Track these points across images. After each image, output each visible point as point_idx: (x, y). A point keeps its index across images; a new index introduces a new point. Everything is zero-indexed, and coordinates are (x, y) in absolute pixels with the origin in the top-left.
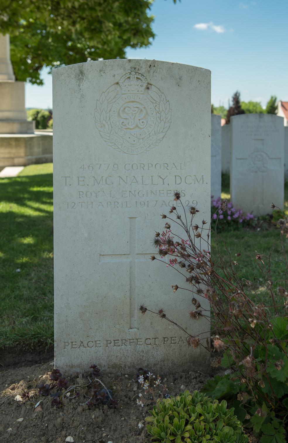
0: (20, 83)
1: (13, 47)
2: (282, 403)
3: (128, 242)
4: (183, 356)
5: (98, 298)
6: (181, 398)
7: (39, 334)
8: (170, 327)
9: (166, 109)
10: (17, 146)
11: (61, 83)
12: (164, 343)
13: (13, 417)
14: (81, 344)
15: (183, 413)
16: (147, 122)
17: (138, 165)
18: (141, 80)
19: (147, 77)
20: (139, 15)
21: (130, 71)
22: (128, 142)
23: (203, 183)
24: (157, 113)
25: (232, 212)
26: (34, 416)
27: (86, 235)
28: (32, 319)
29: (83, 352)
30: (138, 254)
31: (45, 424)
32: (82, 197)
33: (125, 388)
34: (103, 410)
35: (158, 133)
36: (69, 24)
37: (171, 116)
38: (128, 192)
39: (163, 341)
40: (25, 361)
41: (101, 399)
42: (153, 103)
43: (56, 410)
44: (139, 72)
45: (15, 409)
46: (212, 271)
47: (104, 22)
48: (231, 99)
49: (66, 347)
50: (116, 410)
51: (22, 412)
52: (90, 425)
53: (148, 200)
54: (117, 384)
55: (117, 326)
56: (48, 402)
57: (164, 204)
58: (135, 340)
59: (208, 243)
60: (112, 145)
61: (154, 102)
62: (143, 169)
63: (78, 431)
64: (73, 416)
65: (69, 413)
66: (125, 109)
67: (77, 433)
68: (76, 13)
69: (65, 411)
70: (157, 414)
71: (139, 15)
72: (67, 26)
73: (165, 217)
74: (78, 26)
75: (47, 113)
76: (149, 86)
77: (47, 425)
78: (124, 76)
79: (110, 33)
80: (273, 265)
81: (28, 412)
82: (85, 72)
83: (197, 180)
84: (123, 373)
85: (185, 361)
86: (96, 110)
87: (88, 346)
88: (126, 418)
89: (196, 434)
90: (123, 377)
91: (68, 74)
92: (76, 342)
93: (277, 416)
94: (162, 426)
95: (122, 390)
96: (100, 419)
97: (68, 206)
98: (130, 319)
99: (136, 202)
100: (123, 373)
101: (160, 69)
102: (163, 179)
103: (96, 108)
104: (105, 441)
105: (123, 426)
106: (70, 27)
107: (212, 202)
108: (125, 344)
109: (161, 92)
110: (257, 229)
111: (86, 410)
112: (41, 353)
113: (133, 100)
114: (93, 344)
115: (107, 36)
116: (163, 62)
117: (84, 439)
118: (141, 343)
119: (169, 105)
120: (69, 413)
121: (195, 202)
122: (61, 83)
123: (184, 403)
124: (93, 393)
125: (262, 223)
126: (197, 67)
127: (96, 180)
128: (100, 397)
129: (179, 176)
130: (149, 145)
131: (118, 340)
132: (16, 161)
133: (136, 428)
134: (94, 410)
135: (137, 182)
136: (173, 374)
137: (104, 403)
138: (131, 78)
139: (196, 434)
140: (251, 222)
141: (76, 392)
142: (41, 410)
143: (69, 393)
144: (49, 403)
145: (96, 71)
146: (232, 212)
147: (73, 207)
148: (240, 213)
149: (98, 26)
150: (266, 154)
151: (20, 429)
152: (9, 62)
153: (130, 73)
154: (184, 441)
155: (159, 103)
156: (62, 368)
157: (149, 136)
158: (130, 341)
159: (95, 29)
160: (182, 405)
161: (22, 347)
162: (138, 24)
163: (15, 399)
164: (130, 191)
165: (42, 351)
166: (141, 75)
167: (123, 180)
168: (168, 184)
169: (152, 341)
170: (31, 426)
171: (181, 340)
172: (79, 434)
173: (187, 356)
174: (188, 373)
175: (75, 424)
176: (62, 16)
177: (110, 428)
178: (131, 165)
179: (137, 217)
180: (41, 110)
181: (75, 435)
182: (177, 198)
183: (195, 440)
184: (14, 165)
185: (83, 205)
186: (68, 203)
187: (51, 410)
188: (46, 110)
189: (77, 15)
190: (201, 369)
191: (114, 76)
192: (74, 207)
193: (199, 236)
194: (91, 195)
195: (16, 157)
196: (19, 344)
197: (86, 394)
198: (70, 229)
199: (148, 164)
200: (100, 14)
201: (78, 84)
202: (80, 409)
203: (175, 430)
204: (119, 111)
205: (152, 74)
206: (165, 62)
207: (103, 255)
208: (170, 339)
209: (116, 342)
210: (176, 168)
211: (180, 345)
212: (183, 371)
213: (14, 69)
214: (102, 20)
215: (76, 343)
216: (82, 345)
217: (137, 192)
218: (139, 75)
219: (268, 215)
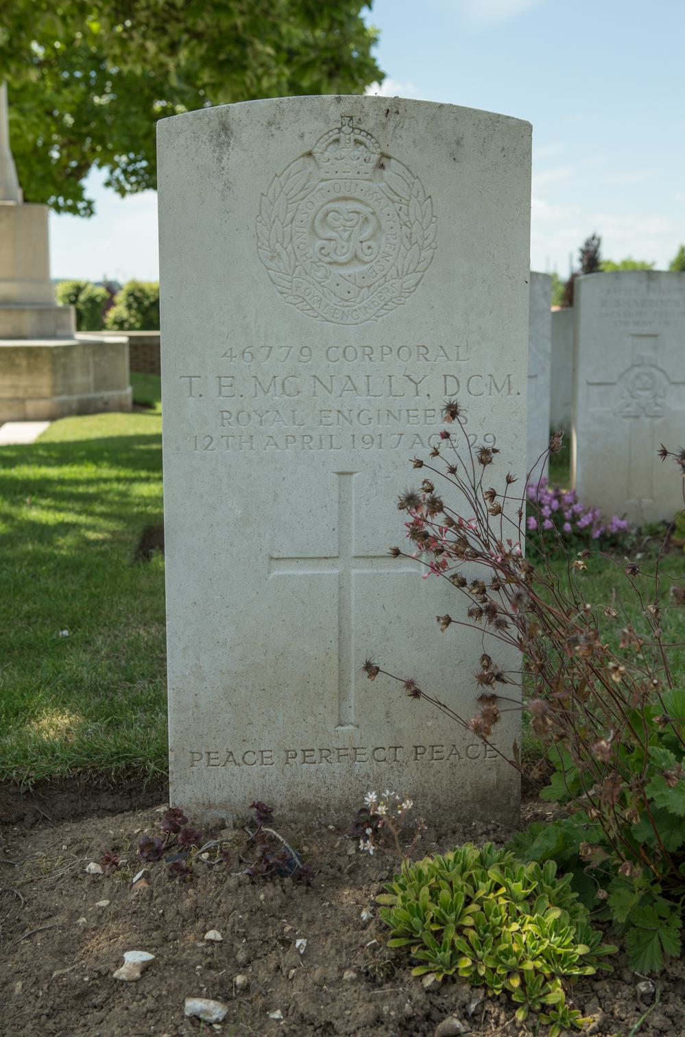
0: (35, 208)
1: (15, 116)
2: (678, 869)
3: (334, 529)
4: (459, 788)
5: (265, 655)
6: (456, 855)
7: (126, 750)
8: (429, 724)
9: (423, 218)
10: (31, 370)
11: (178, 154)
12: (416, 759)
13: (86, 900)
14: (229, 757)
15: (459, 882)
16: (379, 247)
17: (357, 349)
18: (366, 147)
19: (381, 140)
20: (342, 24)
21: (339, 125)
22: (335, 295)
23: (509, 393)
24: (404, 227)
25: (574, 514)
26: (132, 897)
27: (239, 512)
28: (108, 725)
29: (233, 775)
30: (356, 557)
31: (158, 910)
32: (229, 423)
33: (328, 850)
34: (282, 886)
35: (404, 273)
36: (161, 50)
37: (436, 232)
38: (334, 414)
39: (414, 753)
40: (99, 808)
41: (278, 865)
42: (393, 202)
43: (181, 885)
44: (361, 127)
45: (89, 886)
46: (529, 567)
47: (251, 44)
48: (578, 255)
49: (195, 763)
50: (309, 888)
51: (106, 890)
52: (255, 912)
53: (380, 432)
54: (311, 842)
55: (310, 719)
56: (160, 872)
57: (418, 440)
58: (349, 751)
59: (519, 528)
60: (298, 301)
61: (397, 198)
62: (370, 358)
63: (231, 920)
64: (217, 896)
65: (208, 889)
66: (327, 215)
67: (229, 925)
68: (178, 20)
69: (199, 887)
70: (403, 887)
71: (342, 24)
72: (157, 54)
73: (419, 464)
74: (183, 54)
75: (101, 291)
76: (384, 161)
77: (161, 911)
78: (326, 137)
79: (268, 73)
80: (671, 628)
81: (118, 891)
82: (233, 127)
83: (496, 386)
84: (323, 823)
85: (463, 798)
86: (259, 218)
87: (245, 763)
88: (333, 903)
89: (488, 921)
90: (324, 830)
91: (194, 133)
92: (217, 752)
93: (665, 895)
94: (415, 905)
95: (322, 853)
96: (278, 902)
97: (196, 444)
98: (339, 705)
99: (353, 436)
100: (323, 823)
101: (410, 118)
102: (416, 384)
103: (260, 212)
104: (290, 939)
105: (328, 916)
106: (163, 58)
107: (528, 487)
108: (328, 758)
109: (413, 175)
110: (635, 555)
111: (245, 884)
112: (134, 793)
113: (348, 194)
114: (255, 757)
115: (259, 79)
116: (417, 103)
117: (245, 936)
118: (364, 758)
119: (432, 206)
120: (208, 889)
121: (490, 438)
122: (178, 154)
123: (462, 862)
124: (258, 854)
125: (648, 541)
126: (499, 116)
127: (260, 383)
128: (276, 860)
129: (453, 376)
130: (383, 303)
131: (313, 750)
132: (31, 407)
133: (356, 919)
134: (264, 885)
135: (356, 389)
136: (435, 826)
137: (283, 874)
138: (342, 141)
139: (488, 921)
140: (620, 538)
141: (221, 852)
142: (146, 886)
143: (207, 854)
144: (162, 873)
145: (259, 125)
146: (574, 514)
147: (207, 447)
148: (594, 517)
149: (236, 52)
150: (661, 370)
151: (103, 920)
152: (7, 154)
153: (339, 129)
154: (462, 934)
155: (407, 202)
156: (187, 809)
157: (382, 281)
158: (338, 753)
159: (228, 62)
160: (459, 866)
161: (91, 778)
162: (339, 46)
163: (87, 870)
164: (339, 411)
165: (135, 788)
166: (365, 134)
167: (321, 383)
168: (428, 395)
169: (388, 754)
170: (129, 914)
171: (454, 752)
172: (234, 926)
173: (468, 788)
174: (471, 825)
175: (224, 908)
176: (143, 28)
177: (300, 919)
178: (341, 350)
179: (354, 471)
180: (88, 283)
181: (225, 929)
182: (451, 415)
183: (485, 932)
184: (25, 419)
185: (229, 441)
186: (196, 437)
187: (169, 885)
188: (98, 284)
189: (182, 26)
190: (498, 818)
191: (302, 136)
192: (210, 448)
193: (498, 511)
194: (250, 419)
195: (30, 398)
196: (85, 772)
197: (243, 855)
198: (202, 496)
199: (382, 347)
200: (239, 21)
201: (216, 155)
202: (232, 882)
203: (444, 912)
204: (314, 220)
205: (392, 132)
206: (422, 102)
207: (277, 559)
208: (429, 750)
209: (307, 753)
210: (447, 357)
211: (452, 764)
212: (459, 820)
213: (19, 173)
214: (247, 36)
215: (218, 756)
216: (231, 759)
217: (356, 412)
218: (359, 134)
219: (664, 523)
